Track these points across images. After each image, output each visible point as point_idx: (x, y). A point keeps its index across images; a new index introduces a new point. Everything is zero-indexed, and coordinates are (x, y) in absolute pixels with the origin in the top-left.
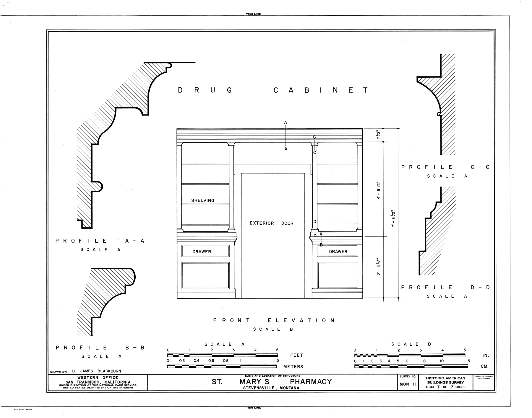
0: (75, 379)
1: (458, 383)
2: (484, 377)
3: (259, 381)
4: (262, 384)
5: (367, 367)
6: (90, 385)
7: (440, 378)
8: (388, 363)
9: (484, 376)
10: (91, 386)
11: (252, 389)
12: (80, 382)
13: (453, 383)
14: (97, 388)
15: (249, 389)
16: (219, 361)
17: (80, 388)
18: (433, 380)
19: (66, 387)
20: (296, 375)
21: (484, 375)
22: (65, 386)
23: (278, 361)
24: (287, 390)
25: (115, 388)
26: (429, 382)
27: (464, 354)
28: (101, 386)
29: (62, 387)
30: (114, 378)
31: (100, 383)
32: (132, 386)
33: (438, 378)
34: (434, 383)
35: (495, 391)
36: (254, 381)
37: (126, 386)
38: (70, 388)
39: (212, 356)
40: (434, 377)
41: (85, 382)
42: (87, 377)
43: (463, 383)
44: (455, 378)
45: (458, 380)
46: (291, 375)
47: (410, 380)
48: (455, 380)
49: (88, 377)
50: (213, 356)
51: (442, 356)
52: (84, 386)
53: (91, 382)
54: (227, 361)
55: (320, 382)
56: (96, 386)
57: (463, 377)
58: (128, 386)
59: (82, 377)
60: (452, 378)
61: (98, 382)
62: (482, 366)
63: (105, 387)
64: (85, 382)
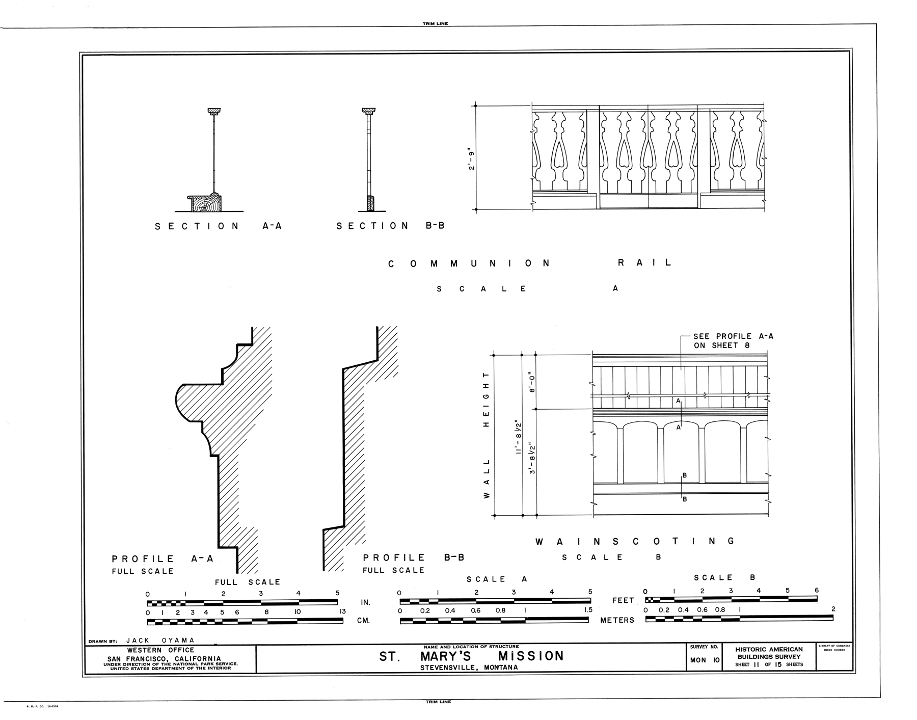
0: (123, 653)
1: (790, 658)
2: (835, 648)
3: (453, 656)
4: (459, 660)
5: (186, 621)
6: (157, 664)
7: (760, 650)
8: (235, 616)
9: (835, 646)
10: (158, 666)
11: (437, 669)
12: (133, 658)
13: (781, 657)
14: (169, 669)
15: (431, 669)
16: (488, 611)
17: (140, 669)
18: (747, 653)
19: (116, 667)
20: (512, 645)
21: (836, 644)
22: (114, 666)
23: (591, 610)
24: (496, 670)
25: (200, 668)
26: (740, 657)
27: (336, 600)
28: (177, 666)
29: (109, 667)
30: (187, 650)
31: (168, 661)
32: (230, 666)
33: (757, 649)
34: (750, 658)
35: (854, 672)
36: (443, 655)
37: (219, 666)
38: (122, 669)
39: (788, 598)
40: (748, 648)
41: (508, 668)
42: (143, 650)
43: (798, 657)
44: (786, 649)
45: (790, 653)
46: (502, 645)
47: (709, 653)
48: (786, 653)
49: (145, 648)
50: (478, 603)
51: (297, 604)
52: (146, 666)
53: (152, 659)
54: (504, 610)
55: (434, 656)
56: (168, 666)
57: (799, 648)
58: (222, 666)
59: (134, 650)
60: (779, 649)
61: (163, 659)
62: (360, 620)
63: (183, 667)
64: (508, 668)
